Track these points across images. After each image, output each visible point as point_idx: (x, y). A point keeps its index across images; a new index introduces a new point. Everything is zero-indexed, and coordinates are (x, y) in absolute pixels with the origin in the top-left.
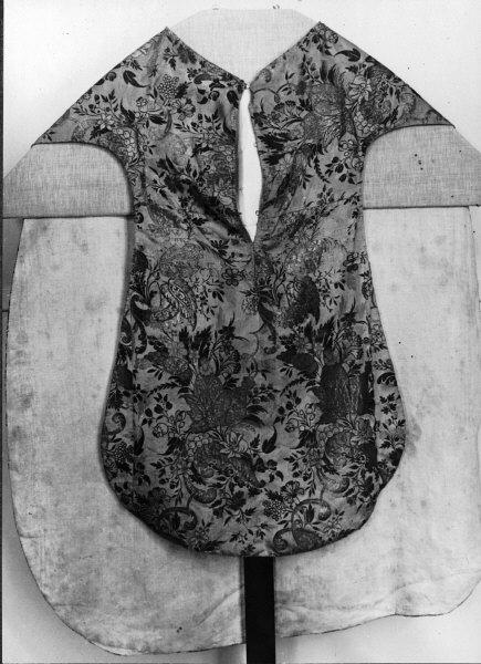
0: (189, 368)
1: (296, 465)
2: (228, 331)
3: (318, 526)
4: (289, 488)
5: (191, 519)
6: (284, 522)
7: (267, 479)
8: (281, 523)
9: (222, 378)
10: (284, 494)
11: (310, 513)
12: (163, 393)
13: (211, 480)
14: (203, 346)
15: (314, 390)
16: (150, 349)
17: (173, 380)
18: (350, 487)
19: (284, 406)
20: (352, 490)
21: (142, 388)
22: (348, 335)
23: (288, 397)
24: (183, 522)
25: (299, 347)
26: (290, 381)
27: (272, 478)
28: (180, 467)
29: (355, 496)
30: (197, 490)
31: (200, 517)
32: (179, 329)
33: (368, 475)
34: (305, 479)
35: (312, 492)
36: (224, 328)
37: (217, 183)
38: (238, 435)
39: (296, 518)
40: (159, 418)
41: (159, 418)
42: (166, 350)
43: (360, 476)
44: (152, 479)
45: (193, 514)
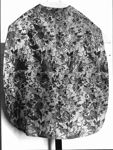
0: (69, 60)
1: (35, 80)
2: (50, 51)
4: (61, 87)
7: (84, 83)
8: (87, 92)
9: (48, 61)
10: (87, 86)
12: (63, 65)
13: (101, 82)
15: (68, 66)
18: (47, 87)
19: (6, 67)
20: (102, 87)
21: (31, 62)
23: (7, 65)
25: (10, 54)
26: (90, 62)
27: (30, 82)
30: (97, 84)
32: (66, 52)
33: (78, 85)
34: (37, 83)
35: (93, 86)
36: (76, 51)
37: (48, 9)
39: (34, 91)
42: (64, 57)
43: (76, 85)
44: (88, 81)
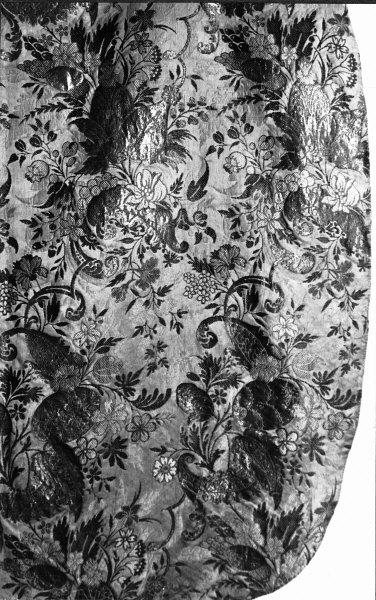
3: (63, 329)
5: (274, 296)
6: (215, 305)
7: (191, 240)
11: (53, 310)
14: (302, 43)
16: (26, 55)
17: (61, 99)
20: (121, 277)
21: (12, 110)
22: (141, 43)
24: (63, 309)
28: (262, 217)
29: (125, 286)
31: (90, 302)
38: (154, 175)
40: (234, 144)
41: (234, 144)
45: (80, 295)
